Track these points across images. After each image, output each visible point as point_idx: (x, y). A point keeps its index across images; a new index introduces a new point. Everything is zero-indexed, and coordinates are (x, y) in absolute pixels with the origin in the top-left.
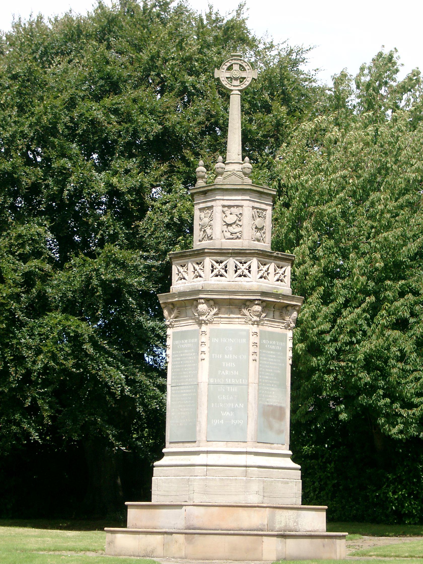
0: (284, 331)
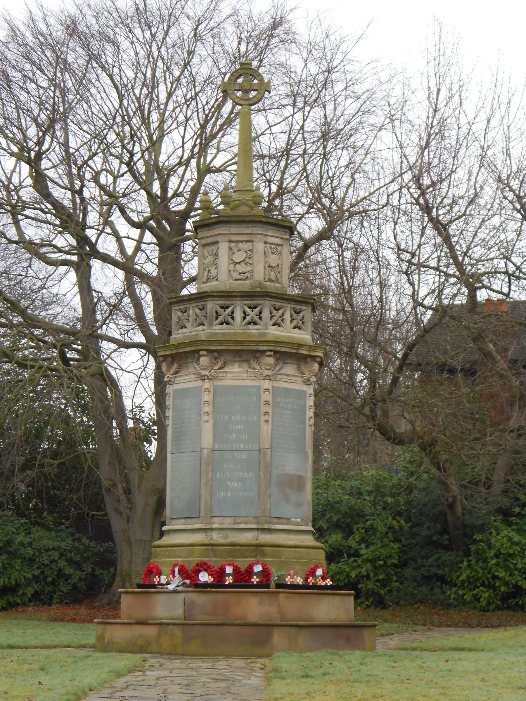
0: (305, 388)
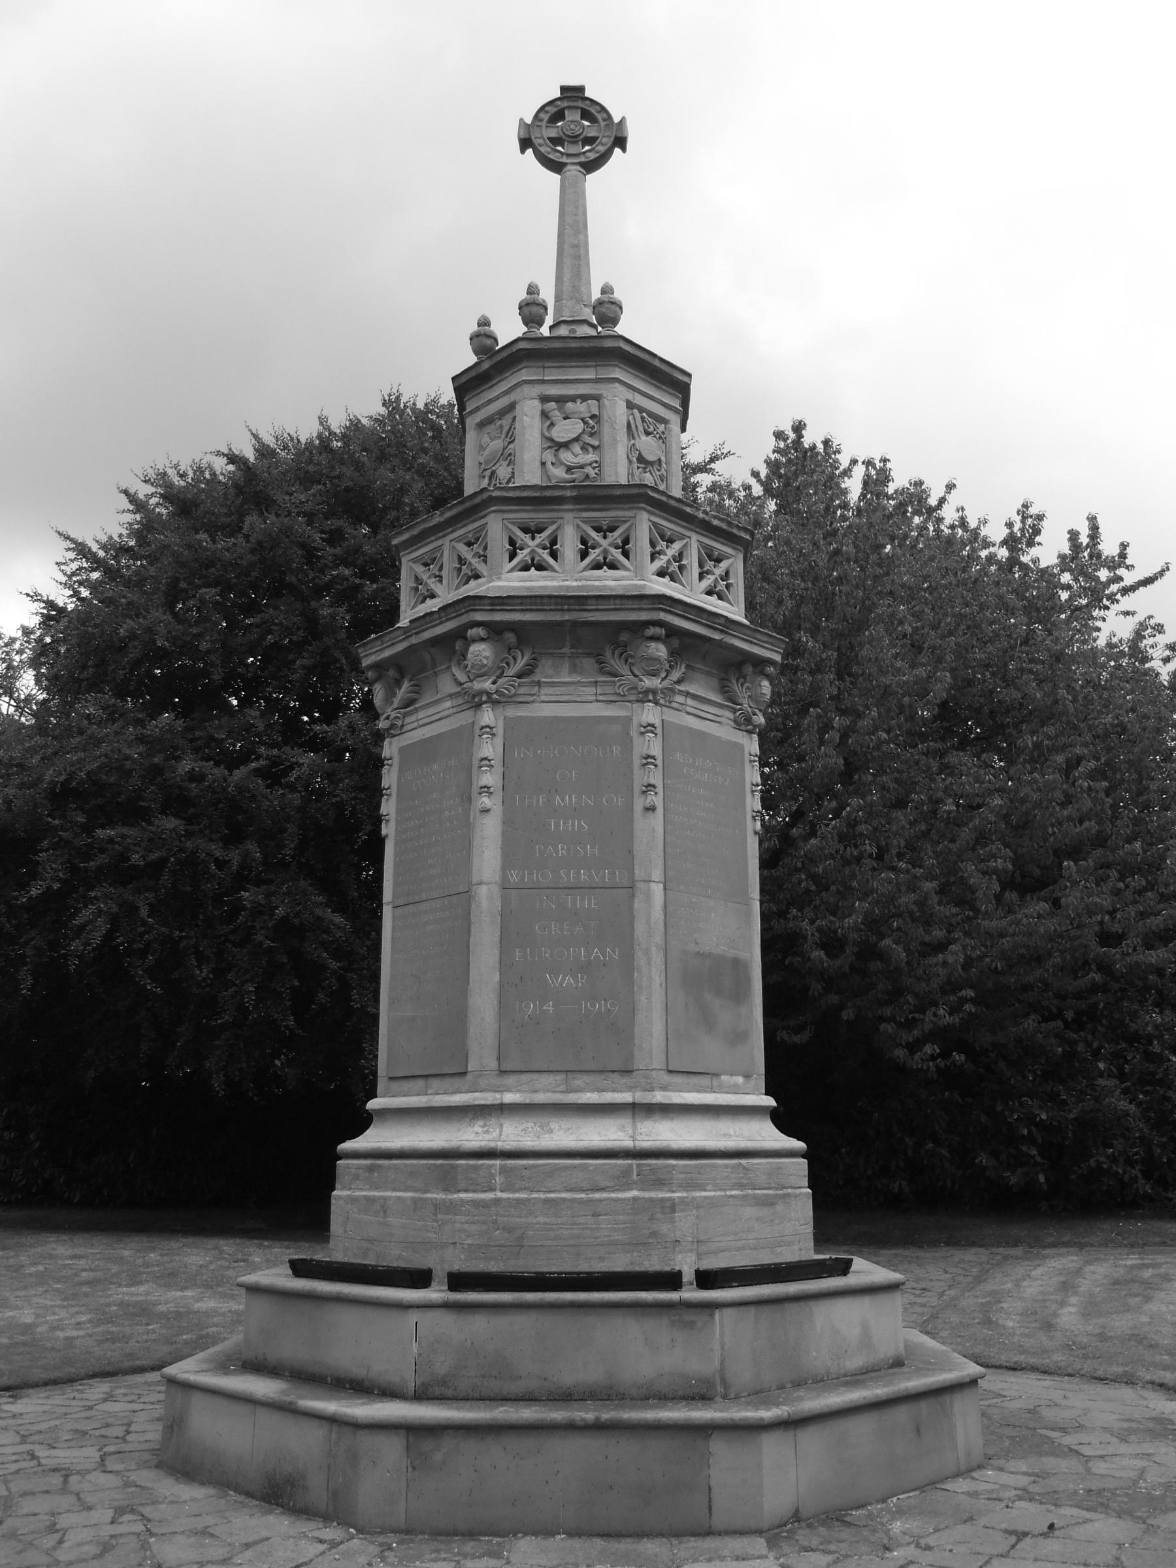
0: (740, 737)
